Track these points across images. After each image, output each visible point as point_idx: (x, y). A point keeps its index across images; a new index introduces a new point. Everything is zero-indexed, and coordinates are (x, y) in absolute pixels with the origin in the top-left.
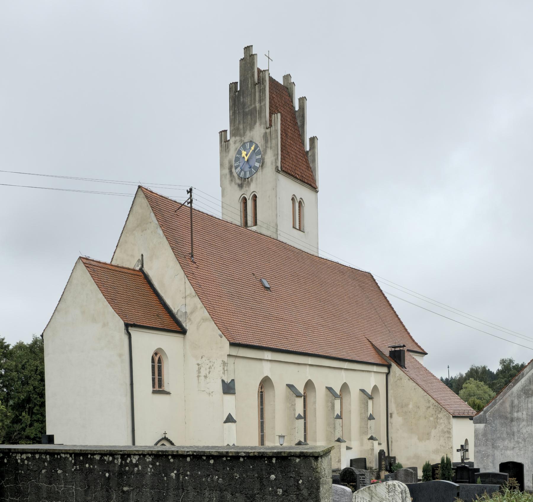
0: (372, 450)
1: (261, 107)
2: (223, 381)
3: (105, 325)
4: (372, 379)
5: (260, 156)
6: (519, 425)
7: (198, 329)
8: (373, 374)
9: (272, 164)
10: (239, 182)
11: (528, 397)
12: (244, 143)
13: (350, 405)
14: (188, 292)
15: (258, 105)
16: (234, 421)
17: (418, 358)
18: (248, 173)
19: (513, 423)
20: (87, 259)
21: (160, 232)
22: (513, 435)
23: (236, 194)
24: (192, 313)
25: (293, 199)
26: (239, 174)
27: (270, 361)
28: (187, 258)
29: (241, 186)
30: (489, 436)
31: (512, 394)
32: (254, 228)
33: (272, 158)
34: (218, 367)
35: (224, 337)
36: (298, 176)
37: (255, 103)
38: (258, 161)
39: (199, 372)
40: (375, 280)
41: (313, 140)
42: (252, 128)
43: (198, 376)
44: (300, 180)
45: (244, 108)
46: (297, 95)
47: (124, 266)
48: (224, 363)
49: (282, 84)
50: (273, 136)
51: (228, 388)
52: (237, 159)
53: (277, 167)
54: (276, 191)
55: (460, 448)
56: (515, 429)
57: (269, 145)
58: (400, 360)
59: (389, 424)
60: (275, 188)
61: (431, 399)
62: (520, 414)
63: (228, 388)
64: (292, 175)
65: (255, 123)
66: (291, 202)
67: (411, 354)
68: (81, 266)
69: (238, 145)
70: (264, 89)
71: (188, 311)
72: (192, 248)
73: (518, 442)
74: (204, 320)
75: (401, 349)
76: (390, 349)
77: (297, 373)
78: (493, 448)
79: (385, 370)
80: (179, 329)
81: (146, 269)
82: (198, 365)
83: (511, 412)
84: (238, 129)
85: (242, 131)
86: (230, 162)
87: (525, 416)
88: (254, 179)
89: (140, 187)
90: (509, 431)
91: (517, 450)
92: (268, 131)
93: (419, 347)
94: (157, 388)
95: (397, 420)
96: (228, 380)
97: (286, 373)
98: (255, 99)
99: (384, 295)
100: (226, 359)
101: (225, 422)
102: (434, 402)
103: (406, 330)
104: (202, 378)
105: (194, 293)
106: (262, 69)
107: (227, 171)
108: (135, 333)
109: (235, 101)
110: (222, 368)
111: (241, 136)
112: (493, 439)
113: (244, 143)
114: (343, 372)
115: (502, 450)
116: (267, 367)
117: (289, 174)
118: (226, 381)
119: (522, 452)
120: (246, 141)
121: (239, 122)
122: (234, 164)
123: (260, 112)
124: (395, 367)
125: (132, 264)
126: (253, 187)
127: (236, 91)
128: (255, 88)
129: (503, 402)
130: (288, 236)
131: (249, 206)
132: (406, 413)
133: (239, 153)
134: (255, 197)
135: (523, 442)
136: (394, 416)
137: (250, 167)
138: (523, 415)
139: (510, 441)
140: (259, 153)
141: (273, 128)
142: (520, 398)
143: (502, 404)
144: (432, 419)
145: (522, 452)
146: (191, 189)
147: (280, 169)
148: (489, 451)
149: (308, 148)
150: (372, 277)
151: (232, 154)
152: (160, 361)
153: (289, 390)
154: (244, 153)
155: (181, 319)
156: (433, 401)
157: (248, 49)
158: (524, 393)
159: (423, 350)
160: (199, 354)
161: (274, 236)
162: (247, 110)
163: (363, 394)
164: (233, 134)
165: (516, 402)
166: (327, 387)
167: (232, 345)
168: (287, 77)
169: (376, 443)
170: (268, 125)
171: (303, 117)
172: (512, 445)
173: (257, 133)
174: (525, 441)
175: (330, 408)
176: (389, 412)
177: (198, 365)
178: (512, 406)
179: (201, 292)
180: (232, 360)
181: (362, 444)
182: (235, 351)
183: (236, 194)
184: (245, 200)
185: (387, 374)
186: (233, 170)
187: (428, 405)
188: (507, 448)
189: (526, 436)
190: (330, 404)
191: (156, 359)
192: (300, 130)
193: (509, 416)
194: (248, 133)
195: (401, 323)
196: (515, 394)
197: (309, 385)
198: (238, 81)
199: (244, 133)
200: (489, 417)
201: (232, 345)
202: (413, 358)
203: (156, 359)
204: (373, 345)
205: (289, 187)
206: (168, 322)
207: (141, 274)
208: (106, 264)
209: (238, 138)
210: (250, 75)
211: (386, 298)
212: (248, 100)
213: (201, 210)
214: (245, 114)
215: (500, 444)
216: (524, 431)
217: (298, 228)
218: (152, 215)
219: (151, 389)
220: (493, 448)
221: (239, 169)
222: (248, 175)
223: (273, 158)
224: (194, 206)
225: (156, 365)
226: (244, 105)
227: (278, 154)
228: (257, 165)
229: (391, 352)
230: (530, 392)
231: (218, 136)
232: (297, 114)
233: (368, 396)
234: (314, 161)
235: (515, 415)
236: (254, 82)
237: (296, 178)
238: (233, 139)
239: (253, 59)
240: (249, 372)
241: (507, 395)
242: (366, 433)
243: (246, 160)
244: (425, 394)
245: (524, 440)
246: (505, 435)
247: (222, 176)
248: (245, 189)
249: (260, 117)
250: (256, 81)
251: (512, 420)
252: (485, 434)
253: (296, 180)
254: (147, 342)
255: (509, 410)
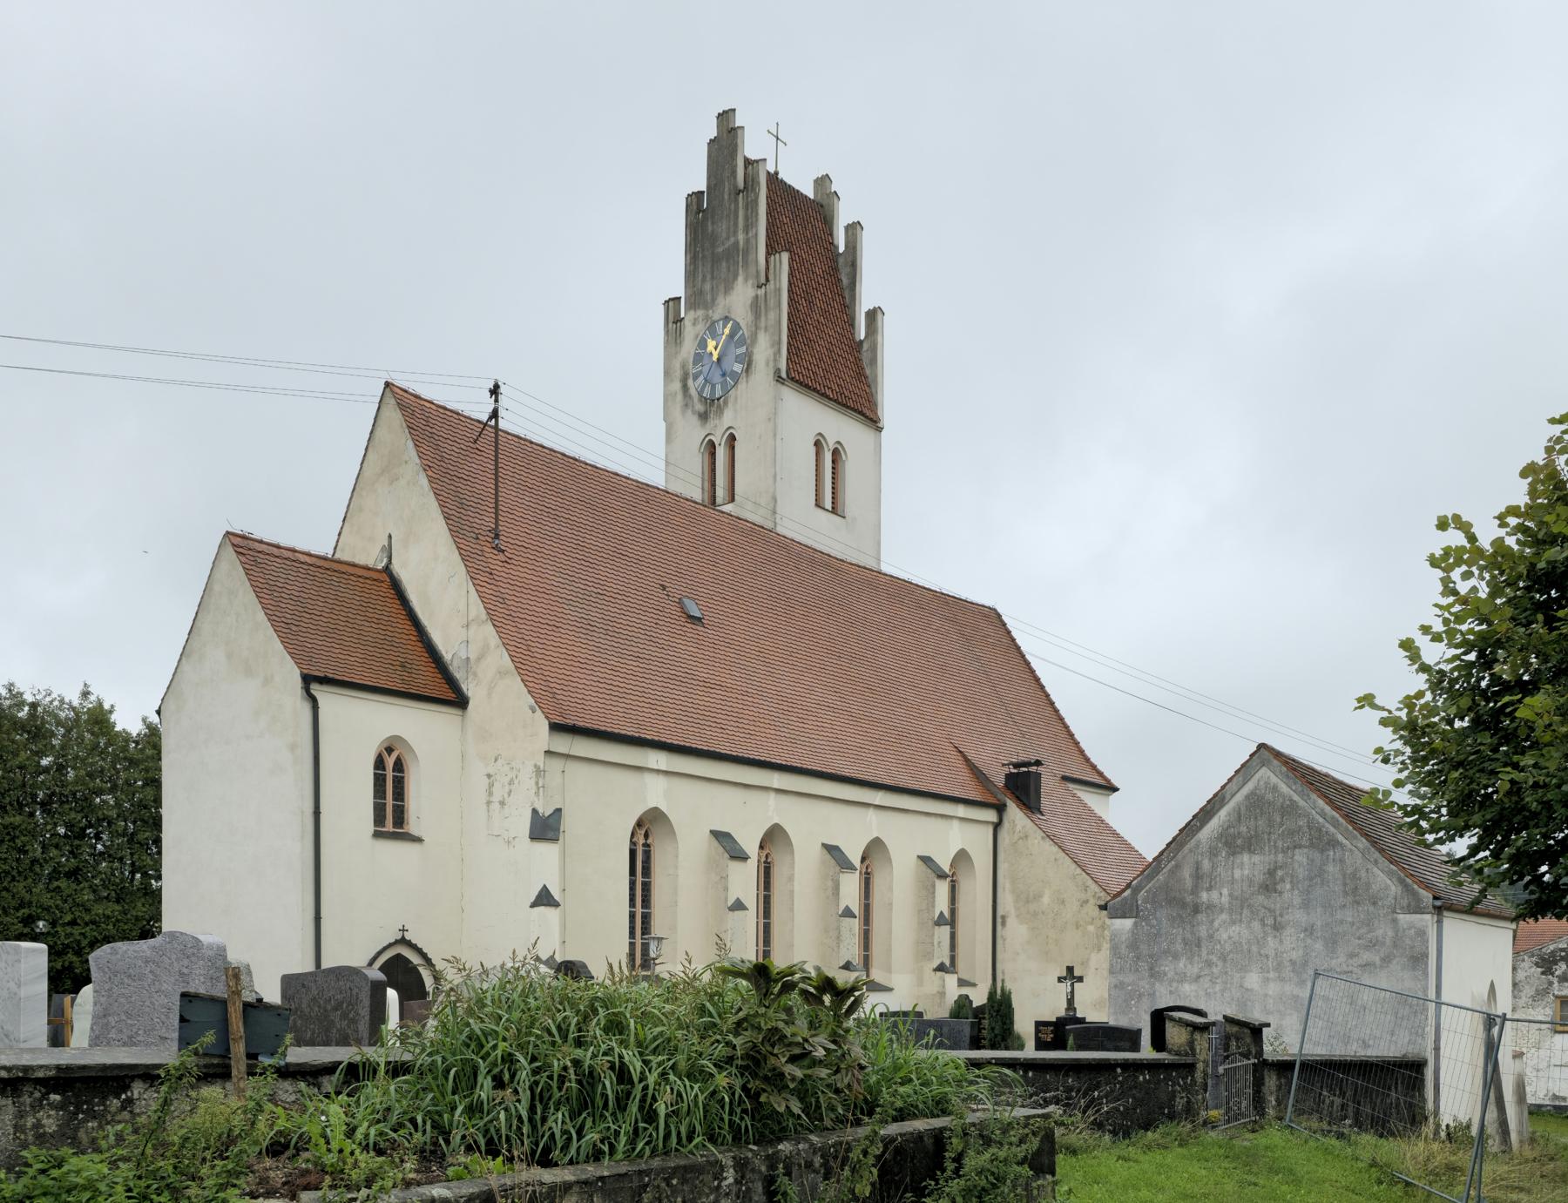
0: (942, 994)
1: (747, 241)
2: (535, 811)
3: (267, 681)
4: (956, 834)
5: (743, 349)
6: (1212, 921)
7: (489, 695)
8: (956, 823)
9: (767, 364)
10: (700, 407)
11: (1234, 854)
12: (713, 323)
13: (891, 889)
14: (472, 615)
15: (741, 237)
16: (556, 905)
17: (1091, 799)
18: (718, 387)
19: (1199, 917)
20: (243, 537)
21: (424, 481)
22: (1199, 946)
23: (693, 434)
24: (479, 659)
25: (817, 444)
26: (701, 391)
27: (666, 773)
28: (481, 542)
29: (704, 417)
30: (1144, 949)
31: (1197, 846)
32: (728, 508)
33: (769, 351)
34: (527, 781)
35: (539, 712)
36: (829, 393)
37: (735, 232)
38: (739, 359)
39: (490, 794)
40: (1004, 625)
41: (872, 315)
42: (728, 289)
43: (489, 803)
44: (835, 401)
45: (713, 246)
46: (843, 219)
47: (357, 561)
48: (539, 772)
49: (812, 196)
50: (772, 303)
51: (545, 828)
52: (698, 358)
53: (778, 371)
54: (782, 426)
55: (1076, 973)
56: (1203, 931)
57: (763, 324)
58: (1027, 794)
59: (999, 941)
60: (773, 418)
61: (1090, 882)
62: (1215, 894)
63: (545, 828)
64: (815, 390)
65: (736, 277)
66: (813, 449)
67: (1071, 786)
68: (230, 552)
69: (701, 327)
70: (756, 201)
71: (472, 657)
72: (497, 519)
73: (1209, 964)
74: (501, 673)
75: (1033, 769)
76: (1006, 770)
77: (748, 810)
78: (1152, 976)
79: (991, 816)
80: (451, 696)
81: (397, 567)
82: (489, 776)
83: (1195, 891)
84: (701, 292)
85: (709, 297)
86: (683, 366)
87: (1225, 900)
88: (731, 401)
89: (387, 384)
90: (1188, 936)
91: (1205, 982)
92: (761, 292)
93: (1101, 774)
94: (389, 826)
95: (1015, 932)
96: (546, 810)
97: (700, 804)
98: (736, 224)
99: (1023, 656)
100: (540, 760)
101: (533, 905)
102: (1097, 889)
103: (1072, 736)
104: (496, 806)
105: (484, 615)
106: (753, 157)
107: (677, 386)
108: (329, 699)
109: (695, 232)
110: (533, 781)
111: (706, 308)
112: (1151, 956)
113: (713, 323)
114: (871, 811)
115: (1172, 981)
116: (656, 785)
117: (807, 386)
118: (541, 811)
119: (1218, 988)
120: (716, 317)
121: (704, 280)
122: (692, 371)
123: (746, 252)
124: (1014, 812)
125: (370, 557)
126: (728, 418)
127: (700, 210)
128: (736, 201)
129: (1177, 866)
130: (802, 522)
131: (718, 456)
132: (1035, 914)
133: (703, 344)
134: (732, 438)
135: (1220, 964)
136: (1009, 921)
137: (724, 375)
138: (1220, 896)
139: (1190, 959)
140: (742, 342)
141: (771, 286)
142: (1216, 855)
143: (1172, 872)
144: (1091, 928)
145: (1218, 988)
146: (497, 386)
147: (784, 375)
148: (1141, 983)
149: (861, 333)
150: (999, 616)
151: (688, 347)
152: (399, 766)
153: (716, 843)
154: (711, 344)
155: (458, 675)
156: (1094, 887)
157: (725, 117)
158: (1226, 844)
159: (1108, 781)
160: (486, 755)
161: (769, 525)
162: (720, 250)
163: (924, 867)
164: (691, 305)
165: (1206, 865)
166: (825, 846)
167: (556, 728)
168: (822, 182)
169: (951, 980)
170: (763, 280)
171: (853, 265)
172: (1194, 970)
173: (739, 298)
174: (1225, 960)
175: (829, 892)
176: (1000, 912)
177: (489, 776)
178: (1198, 876)
179: (500, 612)
180: (556, 765)
181: (920, 982)
182: (564, 744)
183: (693, 434)
184: (711, 448)
185: (997, 826)
186: (690, 382)
187: (1083, 896)
188: (1182, 978)
189: (1228, 947)
190: (830, 883)
191: (390, 762)
192: (847, 294)
193: (1189, 899)
194: (721, 301)
195: (1061, 719)
196: (1204, 848)
197: (774, 837)
198: (704, 188)
199: (713, 300)
200: (1145, 901)
201: (556, 728)
202: (1074, 795)
203: (390, 762)
204: (967, 760)
205: (807, 418)
206: (426, 679)
207: (385, 577)
208: (325, 559)
209: (700, 313)
210: (727, 174)
211: (1028, 664)
212: (722, 228)
213: (809, 543)
214: (716, 260)
215: (1167, 967)
216: (1225, 936)
217: (828, 505)
218: (410, 444)
219: (370, 827)
220: (1152, 976)
221: (701, 379)
222: (718, 393)
223: (771, 352)
224: (502, 424)
225: (390, 774)
226: (713, 239)
227: (779, 343)
228: (738, 368)
229: (1009, 776)
230: (1239, 842)
231: (661, 310)
232: (841, 260)
233: (952, 874)
234: (874, 361)
235: (1204, 896)
236: (735, 186)
237: (824, 395)
238: (692, 314)
239: (735, 137)
240: (608, 796)
241: (1186, 849)
242: (929, 956)
243: (715, 358)
244: (1079, 871)
245: (1224, 958)
246: (1179, 947)
247: (668, 397)
248: (712, 422)
249: (746, 263)
250: (741, 184)
251: (1196, 909)
252: (1134, 945)
253: (826, 401)
254: (360, 724)
255: (1189, 883)
